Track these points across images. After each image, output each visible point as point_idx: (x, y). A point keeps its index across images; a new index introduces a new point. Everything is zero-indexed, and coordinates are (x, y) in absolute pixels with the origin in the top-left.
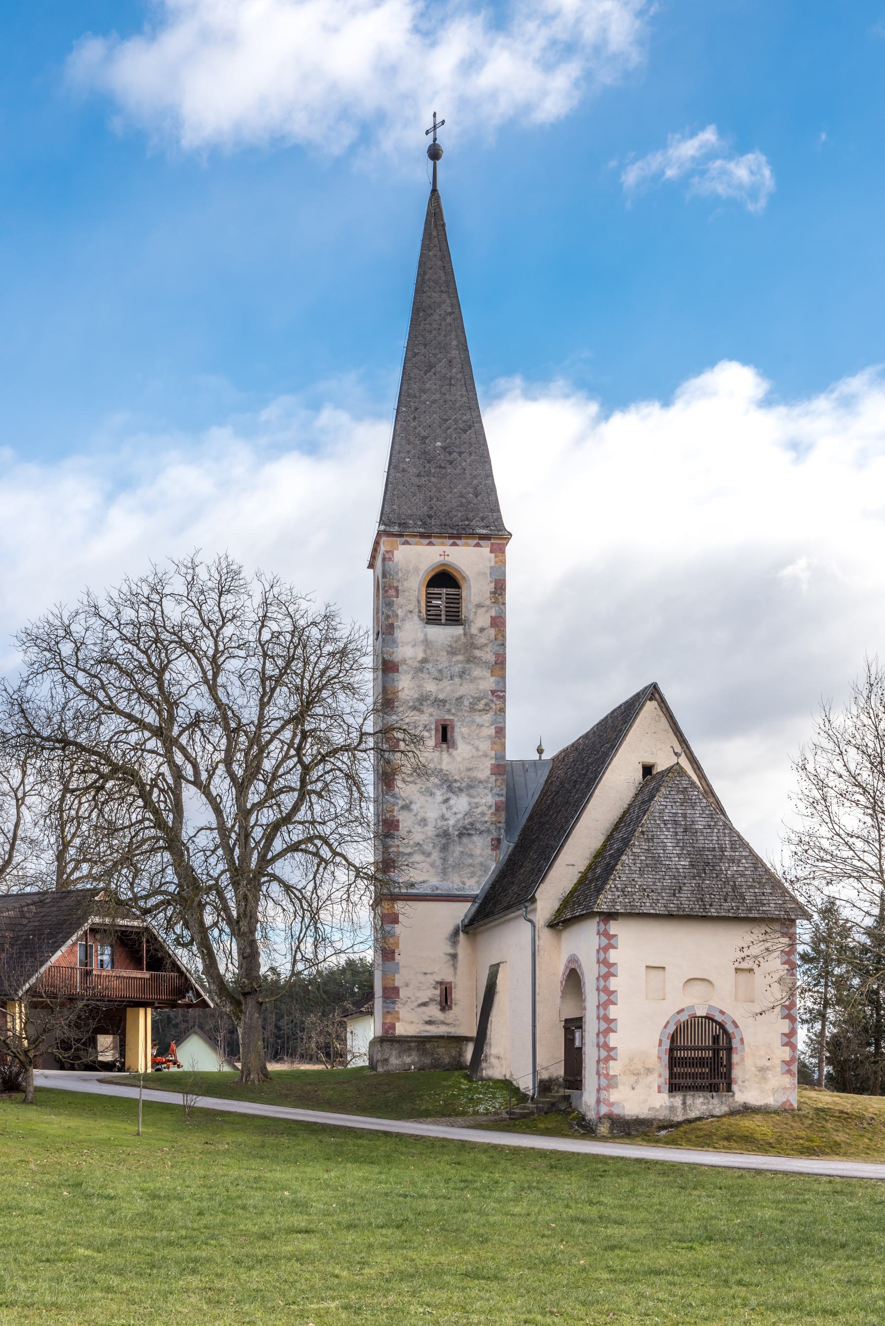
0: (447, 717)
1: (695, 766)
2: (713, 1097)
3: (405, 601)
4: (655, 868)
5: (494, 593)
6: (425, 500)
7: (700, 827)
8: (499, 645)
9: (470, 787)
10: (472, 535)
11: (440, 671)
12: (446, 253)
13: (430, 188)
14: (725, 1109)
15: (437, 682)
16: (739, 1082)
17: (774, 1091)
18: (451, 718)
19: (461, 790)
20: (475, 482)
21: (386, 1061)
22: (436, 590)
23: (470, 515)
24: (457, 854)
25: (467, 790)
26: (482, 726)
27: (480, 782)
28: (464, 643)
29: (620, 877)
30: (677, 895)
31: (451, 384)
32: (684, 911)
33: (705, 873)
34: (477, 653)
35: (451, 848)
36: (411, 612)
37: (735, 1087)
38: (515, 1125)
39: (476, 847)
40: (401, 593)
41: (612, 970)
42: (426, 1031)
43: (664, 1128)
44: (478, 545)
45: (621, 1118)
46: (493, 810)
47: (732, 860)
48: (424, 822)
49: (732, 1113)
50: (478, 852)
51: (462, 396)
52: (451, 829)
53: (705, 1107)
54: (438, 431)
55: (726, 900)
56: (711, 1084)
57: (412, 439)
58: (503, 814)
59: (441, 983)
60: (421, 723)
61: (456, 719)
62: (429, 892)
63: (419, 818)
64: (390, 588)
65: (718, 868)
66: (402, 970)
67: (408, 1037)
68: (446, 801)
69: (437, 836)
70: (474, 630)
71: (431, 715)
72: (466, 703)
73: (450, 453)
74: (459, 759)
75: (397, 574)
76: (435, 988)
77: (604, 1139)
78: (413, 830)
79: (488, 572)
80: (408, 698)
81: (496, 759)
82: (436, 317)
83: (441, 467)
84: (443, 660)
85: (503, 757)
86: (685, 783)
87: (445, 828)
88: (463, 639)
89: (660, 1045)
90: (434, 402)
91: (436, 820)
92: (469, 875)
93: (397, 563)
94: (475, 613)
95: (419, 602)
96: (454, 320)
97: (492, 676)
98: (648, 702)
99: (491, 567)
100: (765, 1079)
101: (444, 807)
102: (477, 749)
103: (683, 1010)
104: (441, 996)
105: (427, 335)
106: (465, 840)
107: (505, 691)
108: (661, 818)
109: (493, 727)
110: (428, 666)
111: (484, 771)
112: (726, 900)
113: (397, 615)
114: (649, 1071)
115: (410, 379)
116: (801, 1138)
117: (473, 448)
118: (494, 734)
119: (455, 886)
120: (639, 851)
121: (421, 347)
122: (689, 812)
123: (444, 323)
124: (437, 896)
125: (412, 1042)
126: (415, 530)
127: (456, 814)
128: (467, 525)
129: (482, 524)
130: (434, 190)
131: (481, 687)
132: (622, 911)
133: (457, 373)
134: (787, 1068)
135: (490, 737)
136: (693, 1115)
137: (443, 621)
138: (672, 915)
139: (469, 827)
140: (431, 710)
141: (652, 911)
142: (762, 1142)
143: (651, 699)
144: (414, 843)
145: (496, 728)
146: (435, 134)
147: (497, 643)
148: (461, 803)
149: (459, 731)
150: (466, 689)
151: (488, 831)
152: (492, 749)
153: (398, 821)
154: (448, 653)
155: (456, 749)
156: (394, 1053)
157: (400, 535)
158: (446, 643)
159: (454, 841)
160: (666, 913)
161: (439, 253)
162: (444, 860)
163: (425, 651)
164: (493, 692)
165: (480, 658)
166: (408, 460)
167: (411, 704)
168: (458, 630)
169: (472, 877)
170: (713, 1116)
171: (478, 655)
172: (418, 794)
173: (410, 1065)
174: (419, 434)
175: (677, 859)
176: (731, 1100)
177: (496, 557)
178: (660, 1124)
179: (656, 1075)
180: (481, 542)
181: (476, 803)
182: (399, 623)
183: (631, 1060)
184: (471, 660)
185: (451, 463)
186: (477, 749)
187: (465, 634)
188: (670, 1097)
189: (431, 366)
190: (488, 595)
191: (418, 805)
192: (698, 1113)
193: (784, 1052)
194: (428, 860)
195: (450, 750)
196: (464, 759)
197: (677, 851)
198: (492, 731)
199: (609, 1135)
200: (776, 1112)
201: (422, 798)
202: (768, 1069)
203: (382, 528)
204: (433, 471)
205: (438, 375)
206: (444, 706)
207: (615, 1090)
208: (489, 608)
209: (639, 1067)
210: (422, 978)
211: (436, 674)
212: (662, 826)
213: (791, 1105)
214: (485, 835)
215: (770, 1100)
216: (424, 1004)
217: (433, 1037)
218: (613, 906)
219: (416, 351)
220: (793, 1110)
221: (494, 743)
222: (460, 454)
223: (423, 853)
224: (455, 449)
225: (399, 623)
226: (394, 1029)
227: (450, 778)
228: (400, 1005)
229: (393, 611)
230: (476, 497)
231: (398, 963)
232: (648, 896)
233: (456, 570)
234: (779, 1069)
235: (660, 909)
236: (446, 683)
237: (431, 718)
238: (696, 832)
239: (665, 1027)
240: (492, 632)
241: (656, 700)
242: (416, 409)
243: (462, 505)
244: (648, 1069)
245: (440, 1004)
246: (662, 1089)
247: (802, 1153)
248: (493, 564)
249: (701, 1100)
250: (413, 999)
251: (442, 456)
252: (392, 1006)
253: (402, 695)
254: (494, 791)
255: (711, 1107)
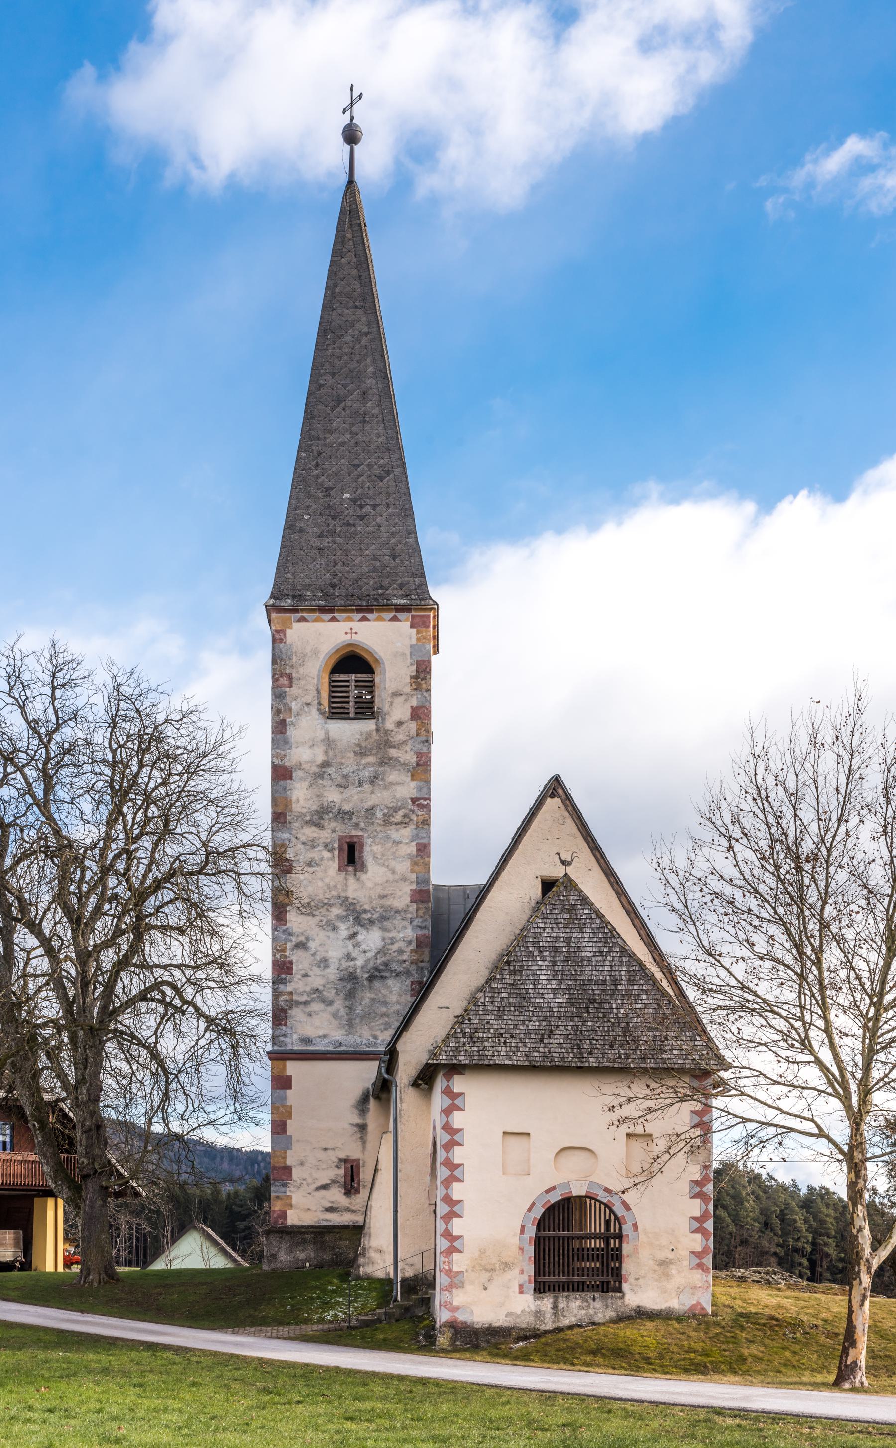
0: (354, 833)
1: (612, 879)
2: (594, 1299)
3: (300, 691)
4: (519, 1008)
5: (416, 677)
6: (327, 566)
7: (588, 954)
8: (422, 742)
9: (383, 918)
10: (387, 607)
11: (346, 777)
12: (363, 259)
13: (345, 178)
14: (611, 1314)
15: (342, 790)
16: (631, 1279)
17: (680, 1291)
18: (360, 833)
19: (371, 922)
20: (393, 541)
21: (274, 1256)
22: (343, 677)
23: (386, 582)
24: (366, 1001)
25: (380, 922)
26: (400, 842)
27: (397, 912)
28: (377, 741)
29: (470, 1020)
30: (546, 1041)
31: (365, 421)
32: (552, 1060)
33: (588, 1012)
34: (393, 752)
35: (359, 994)
36: (308, 704)
37: (625, 1287)
38: (351, 1334)
39: (391, 992)
40: (295, 682)
41: (456, 1138)
42: (327, 1220)
43: (525, 1338)
44: (394, 619)
45: (468, 1326)
46: (413, 946)
47: (627, 995)
48: (324, 962)
49: (620, 1319)
50: (394, 998)
51: (378, 435)
52: (358, 970)
53: (583, 1312)
54: (347, 480)
55: (612, 1047)
56: (603, 1283)
57: (312, 491)
58: (427, 951)
59: (346, 1161)
60: (321, 841)
61: (366, 835)
62: (331, 1048)
63: (318, 958)
64: (281, 676)
65: (607, 1006)
66: (295, 1146)
67: (303, 1227)
68: (353, 936)
69: (341, 979)
70: (389, 725)
71: (334, 831)
72: (379, 815)
73: (361, 507)
74: (369, 884)
75: (290, 659)
76: (338, 1167)
77: (444, 1352)
78: (310, 973)
79: (408, 652)
80: (304, 811)
81: (418, 883)
82: (348, 339)
83: (349, 524)
84: (350, 763)
85: (427, 881)
86: (573, 899)
87: (351, 970)
88: (376, 736)
89: (522, 1232)
90: (343, 444)
91: (340, 960)
92: (382, 1027)
93: (291, 645)
94: (391, 704)
95: (318, 692)
96: (372, 341)
97: (413, 780)
98: (549, 800)
99: (412, 646)
100: (667, 1276)
101: (350, 944)
102: (393, 872)
103: (554, 1188)
104: (345, 1176)
105: (336, 361)
106: (377, 984)
107: (429, 799)
108: (535, 944)
109: (414, 844)
110: (329, 770)
111: (402, 898)
112: (612, 1047)
113: (290, 710)
114: (507, 1266)
115: (313, 417)
116: (695, 1352)
117: (391, 499)
118: (414, 852)
119: (365, 1041)
120: (501, 986)
121: (328, 377)
122: (575, 935)
123: (358, 347)
124: (346, 1053)
125: (307, 1233)
126: (314, 603)
127: (365, 952)
128: (381, 595)
129: (401, 593)
130: (351, 182)
131: (398, 795)
132: (467, 1062)
133: (373, 408)
134: (698, 1261)
135: (410, 856)
136: (566, 1322)
137: (352, 715)
138: (534, 1066)
139: (382, 967)
140: (333, 824)
141: (507, 1062)
142: (637, 1357)
143: (552, 796)
144: (312, 989)
145: (417, 844)
146: (352, 112)
147: (419, 739)
148: (372, 939)
149: (370, 850)
150: (380, 798)
151: (407, 973)
152: (412, 871)
153: (291, 962)
154: (356, 753)
155: (366, 872)
156: (284, 1247)
157: (295, 611)
158: (353, 741)
159: (363, 986)
160: (527, 1063)
161: (354, 260)
162: (350, 1009)
163: (326, 752)
164: (414, 801)
165: (397, 759)
166: (306, 517)
167: (308, 818)
168: (369, 725)
169: (386, 1029)
170: (594, 1323)
171: (395, 755)
172: (317, 929)
173: (304, 1261)
174: (322, 485)
175: (551, 995)
176: (619, 1302)
177: (418, 632)
178: (521, 1334)
179: (516, 1271)
180: (399, 615)
181: (392, 939)
182: (292, 719)
183: (482, 1252)
184: (385, 761)
185: (362, 518)
186: (393, 872)
187: (378, 730)
188: (536, 1299)
189: (339, 400)
190: (408, 680)
191: (317, 942)
192: (573, 1319)
193: (694, 1240)
194: (329, 1009)
195: (358, 873)
196: (376, 884)
197: (554, 985)
198: (412, 849)
199: (450, 1348)
200: (679, 1319)
201: (322, 934)
202: (671, 1262)
203: (272, 601)
204: (339, 529)
205: (348, 411)
206: (351, 819)
207: (460, 1290)
208: (409, 696)
209: (494, 1261)
210: (322, 1155)
211: (340, 780)
212: (536, 953)
213: (703, 1308)
214: (403, 977)
215: (676, 1303)
216: (324, 1187)
217: (334, 1227)
218: (455, 1056)
219: (321, 382)
220: (705, 1315)
221: (415, 864)
222: (374, 507)
223: (323, 1001)
224: (368, 500)
225: (292, 719)
226: (285, 1218)
227: (358, 908)
228: (292, 1189)
229: (285, 705)
230: (394, 559)
231: (290, 1137)
232: (505, 1043)
233: (367, 650)
234: (686, 1263)
235: (519, 1059)
236: (352, 791)
237: (334, 835)
238: (582, 961)
239: (529, 1210)
240: (413, 726)
241: (559, 797)
242: (319, 454)
243: (375, 570)
244: (506, 1264)
245: (345, 1186)
246: (524, 1289)
247: (687, 1371)
248: (414, 641)
249: (578, 1302)
250: (309, 1180)
251: (351, 511)
252: (283, 1189)
253: (297, 808)
254: (415, 923)
255: (591, 1311)
